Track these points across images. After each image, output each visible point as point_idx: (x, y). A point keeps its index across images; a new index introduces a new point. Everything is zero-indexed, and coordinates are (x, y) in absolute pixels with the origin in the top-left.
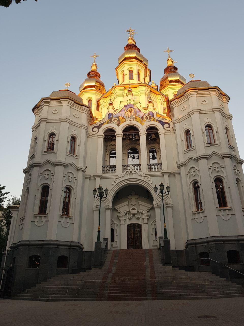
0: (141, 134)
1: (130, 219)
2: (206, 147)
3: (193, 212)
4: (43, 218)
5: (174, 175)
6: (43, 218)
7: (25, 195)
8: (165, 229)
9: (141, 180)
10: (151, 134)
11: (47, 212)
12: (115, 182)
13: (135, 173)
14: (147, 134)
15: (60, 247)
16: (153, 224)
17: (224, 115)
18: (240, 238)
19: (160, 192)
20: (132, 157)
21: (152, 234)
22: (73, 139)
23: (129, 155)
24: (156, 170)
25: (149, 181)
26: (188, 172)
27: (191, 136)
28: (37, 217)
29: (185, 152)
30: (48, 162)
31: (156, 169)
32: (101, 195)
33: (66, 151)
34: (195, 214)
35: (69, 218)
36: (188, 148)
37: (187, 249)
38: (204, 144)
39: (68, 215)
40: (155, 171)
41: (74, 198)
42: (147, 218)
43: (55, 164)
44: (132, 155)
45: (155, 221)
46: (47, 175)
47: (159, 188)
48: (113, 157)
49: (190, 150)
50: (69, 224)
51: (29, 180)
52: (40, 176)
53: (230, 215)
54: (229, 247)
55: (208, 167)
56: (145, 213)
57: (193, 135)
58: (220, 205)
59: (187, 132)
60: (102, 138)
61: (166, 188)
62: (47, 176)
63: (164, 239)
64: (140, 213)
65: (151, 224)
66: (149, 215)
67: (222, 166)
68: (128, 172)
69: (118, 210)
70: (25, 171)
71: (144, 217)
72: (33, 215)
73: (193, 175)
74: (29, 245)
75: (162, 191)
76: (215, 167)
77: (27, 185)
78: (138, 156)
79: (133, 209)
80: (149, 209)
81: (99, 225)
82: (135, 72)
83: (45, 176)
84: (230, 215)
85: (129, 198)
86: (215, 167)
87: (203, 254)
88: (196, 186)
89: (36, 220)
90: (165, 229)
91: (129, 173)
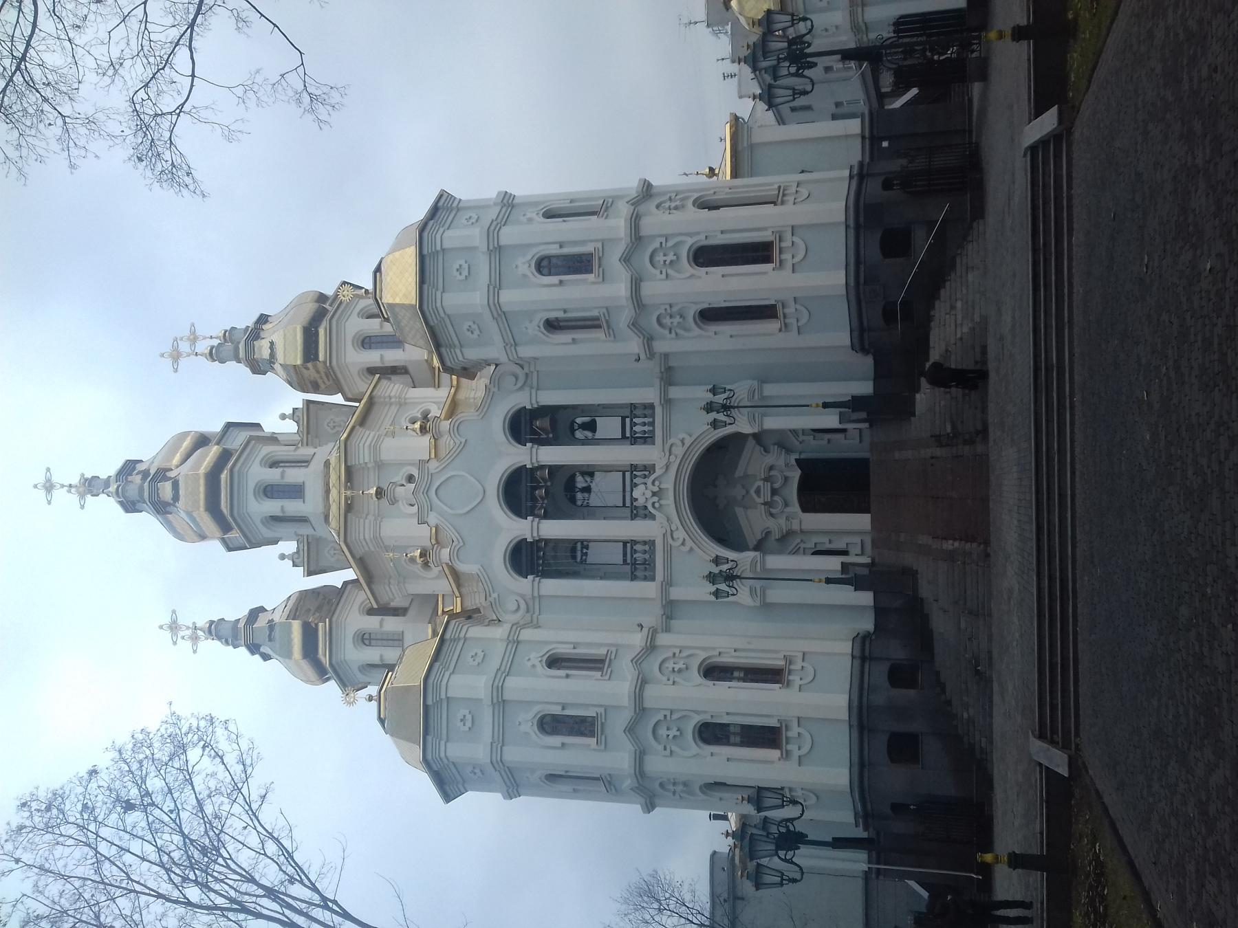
0: (534, 460)
1: (786, 504)
2: (603, 280)
3: (780, 330)
4: (790, 734)
5: (669, 369)
6: (790, 734)
7: (721, 799)
8: (826, 405)
9: (679, 466)
10: (533, 432)
11: (773, 723)
12: (683, 544)
13: (657, 483)
14: (532, 441)
15: (866, 686)
16: (800, 439)
17: (503, 217)
18: (851, 223)
19: (725, 413)
20: (586, 495)
21: (829, 441)
22: (554, 662)
23: (579, 503)
24: (651, 420)
25: (683, 444)
26: (670, 332)
27: (566, 315)
28: (787, 751)
29: (610, 336)
30: (626, 259)
31: (646, 420)
32: (730, 577)
33: (597, 680)
34: (786, 325)
35: (790, 664)
36: (599, 327)
37: (872, 350)
38: (593, 283)
39: (783, 670)
40: (652, 424)
41: (735, 654)
42: (783, 453)
43: (641, 710)
44: (579, 496)
45: (794, 432)
46: (668, 732)
47: (714, 415)
48: (585, 551)
49: (607, 322)
50: (804, 664)
51: (680, 788)
52: (671, 751)
53: (796, 239)
54: (873, 251)
55: (662, 280)
56: (770, 459)
57: (565, 311)
58: (767, 259)
59: (552, 325)
60: (539, 582)
61: (714, 395)
62: (673, 732)
63: (850, 410)
64: (771, 474)
65: (801, 443)
66: (776, 447)
67: (661, 243)
68: (653, 503)
69: (759, 537)
70: (649, 807)
71: (781, 462)
72: (781, 762)
73: (681, 320)
74: (862, 765)
75: (726, 408)
76: (665, 261)
77: (691, 793)
78: (583, 474)
79: (758, 492)
80: (758, 447)
81: (811, 580)
82: (273, 475)
83: (671, 737)
84: (796, 239)
85: (743, 496)
86: (665, 261)
87: (889, 315)
88: (710, 316)
89: (796, 753)
90: (826, 405)
91: (658, 502)
